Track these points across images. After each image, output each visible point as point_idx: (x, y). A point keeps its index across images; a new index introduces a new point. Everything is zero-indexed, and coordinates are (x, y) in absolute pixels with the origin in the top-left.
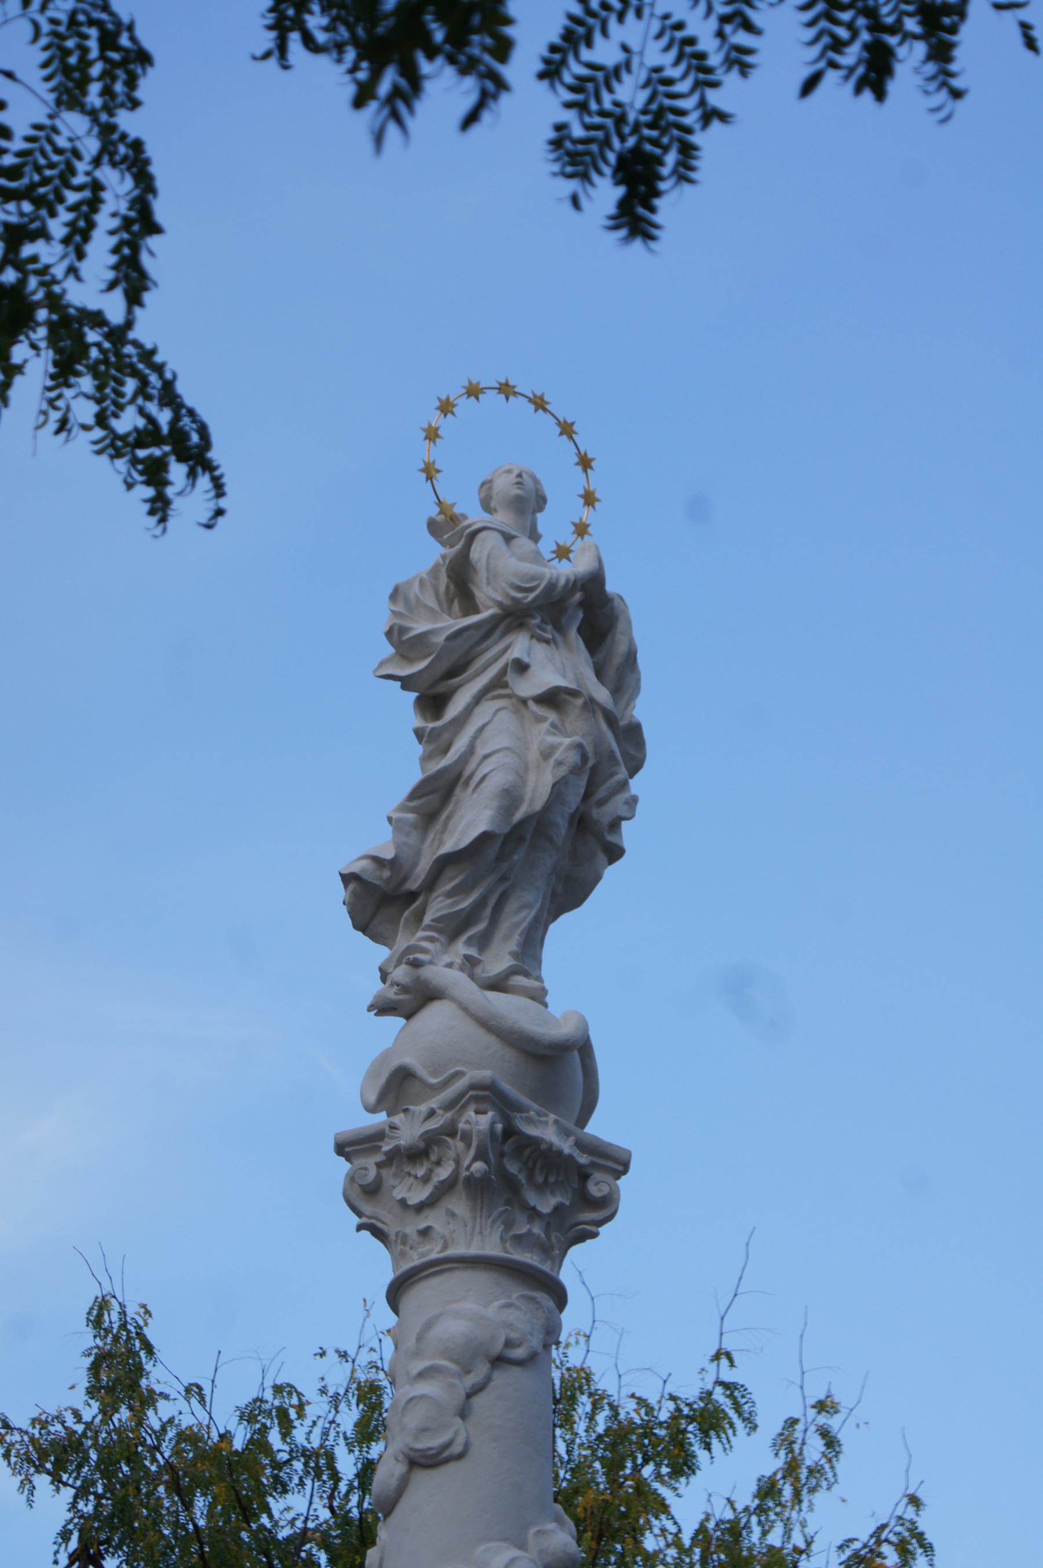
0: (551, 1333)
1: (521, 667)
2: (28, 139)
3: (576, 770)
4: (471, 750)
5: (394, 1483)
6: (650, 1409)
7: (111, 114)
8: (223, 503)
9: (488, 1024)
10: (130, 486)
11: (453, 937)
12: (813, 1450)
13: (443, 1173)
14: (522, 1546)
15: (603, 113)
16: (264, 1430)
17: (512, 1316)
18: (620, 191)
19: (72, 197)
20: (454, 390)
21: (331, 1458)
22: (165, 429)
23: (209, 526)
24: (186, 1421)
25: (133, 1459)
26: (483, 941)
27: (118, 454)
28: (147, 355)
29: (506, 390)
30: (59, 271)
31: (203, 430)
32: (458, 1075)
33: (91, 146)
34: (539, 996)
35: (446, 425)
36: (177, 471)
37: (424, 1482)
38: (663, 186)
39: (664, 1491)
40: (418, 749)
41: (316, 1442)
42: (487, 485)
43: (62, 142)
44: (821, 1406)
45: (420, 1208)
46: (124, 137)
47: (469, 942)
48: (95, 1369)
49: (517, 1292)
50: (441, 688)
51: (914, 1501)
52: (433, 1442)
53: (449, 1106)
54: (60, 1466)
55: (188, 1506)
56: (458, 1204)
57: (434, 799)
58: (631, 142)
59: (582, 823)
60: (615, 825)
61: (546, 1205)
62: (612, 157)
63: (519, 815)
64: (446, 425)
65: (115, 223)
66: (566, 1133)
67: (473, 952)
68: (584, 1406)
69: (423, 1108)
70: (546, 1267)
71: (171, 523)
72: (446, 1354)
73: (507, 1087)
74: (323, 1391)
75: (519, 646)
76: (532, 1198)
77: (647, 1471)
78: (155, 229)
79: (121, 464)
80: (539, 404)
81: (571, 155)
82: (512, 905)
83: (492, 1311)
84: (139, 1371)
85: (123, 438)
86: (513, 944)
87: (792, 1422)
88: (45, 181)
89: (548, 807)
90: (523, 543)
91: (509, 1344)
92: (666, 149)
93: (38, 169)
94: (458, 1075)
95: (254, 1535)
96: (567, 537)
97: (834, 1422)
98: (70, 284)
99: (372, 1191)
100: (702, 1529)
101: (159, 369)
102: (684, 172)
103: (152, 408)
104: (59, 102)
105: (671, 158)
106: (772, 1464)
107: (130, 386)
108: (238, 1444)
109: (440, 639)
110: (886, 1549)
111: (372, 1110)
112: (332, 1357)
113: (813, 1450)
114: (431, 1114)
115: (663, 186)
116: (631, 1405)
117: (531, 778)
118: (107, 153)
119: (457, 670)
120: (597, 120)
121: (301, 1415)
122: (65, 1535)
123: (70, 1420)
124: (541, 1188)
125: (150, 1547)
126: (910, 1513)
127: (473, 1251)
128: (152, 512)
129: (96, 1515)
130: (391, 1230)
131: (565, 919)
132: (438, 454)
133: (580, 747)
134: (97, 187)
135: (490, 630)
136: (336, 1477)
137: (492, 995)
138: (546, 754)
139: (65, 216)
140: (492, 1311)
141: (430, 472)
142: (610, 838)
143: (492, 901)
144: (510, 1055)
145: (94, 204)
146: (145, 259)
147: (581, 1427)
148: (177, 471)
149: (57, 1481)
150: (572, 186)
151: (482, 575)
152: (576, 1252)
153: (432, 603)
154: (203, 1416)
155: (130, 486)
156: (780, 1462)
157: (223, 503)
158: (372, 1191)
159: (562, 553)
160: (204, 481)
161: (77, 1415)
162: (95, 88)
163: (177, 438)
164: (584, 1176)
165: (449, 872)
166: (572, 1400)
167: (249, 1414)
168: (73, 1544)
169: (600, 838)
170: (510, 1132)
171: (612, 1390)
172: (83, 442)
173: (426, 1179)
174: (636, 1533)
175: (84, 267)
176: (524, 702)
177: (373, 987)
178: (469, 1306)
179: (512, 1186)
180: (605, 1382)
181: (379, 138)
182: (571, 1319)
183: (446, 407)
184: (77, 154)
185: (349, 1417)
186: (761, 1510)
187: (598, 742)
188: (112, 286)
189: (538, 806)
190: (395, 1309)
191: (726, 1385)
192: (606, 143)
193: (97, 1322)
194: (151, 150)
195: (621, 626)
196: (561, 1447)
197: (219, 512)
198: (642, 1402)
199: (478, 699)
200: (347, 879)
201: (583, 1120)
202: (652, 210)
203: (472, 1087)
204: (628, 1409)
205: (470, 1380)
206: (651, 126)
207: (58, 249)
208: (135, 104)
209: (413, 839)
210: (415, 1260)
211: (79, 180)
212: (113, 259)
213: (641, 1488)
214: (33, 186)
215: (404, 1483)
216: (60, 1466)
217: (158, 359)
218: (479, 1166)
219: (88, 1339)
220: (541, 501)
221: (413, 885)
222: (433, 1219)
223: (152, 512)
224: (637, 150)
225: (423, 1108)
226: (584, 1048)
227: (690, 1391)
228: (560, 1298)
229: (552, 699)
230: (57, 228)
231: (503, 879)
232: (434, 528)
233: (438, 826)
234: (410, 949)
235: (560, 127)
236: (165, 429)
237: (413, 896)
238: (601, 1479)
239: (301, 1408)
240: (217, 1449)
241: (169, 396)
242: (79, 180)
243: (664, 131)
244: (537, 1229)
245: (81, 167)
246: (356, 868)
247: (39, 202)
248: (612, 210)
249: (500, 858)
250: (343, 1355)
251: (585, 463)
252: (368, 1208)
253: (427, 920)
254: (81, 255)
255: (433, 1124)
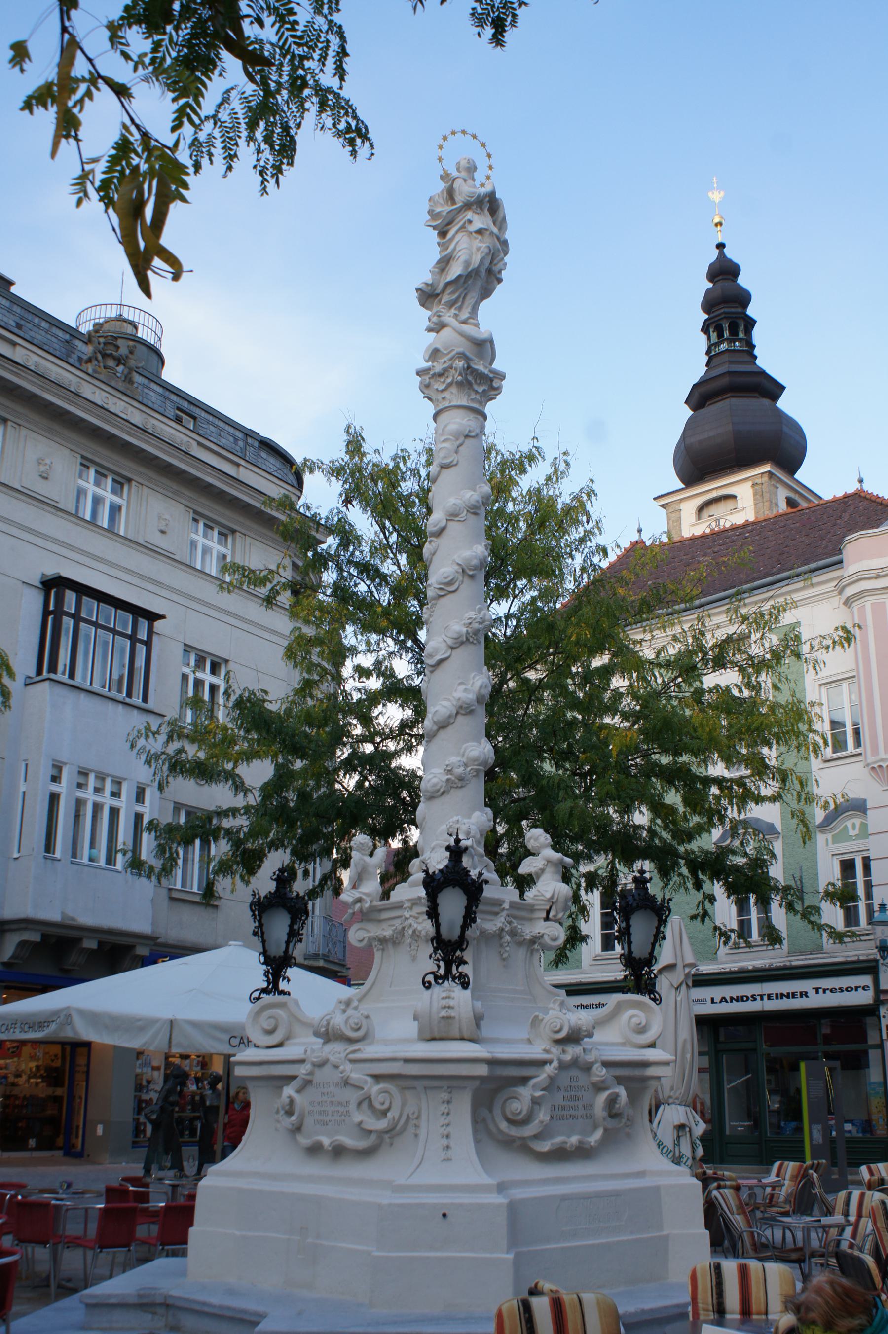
0: (483, 427)
1: (470, 222)
2: (305, 26)
3: (488, 254)
4: (455, 249)
5: (436, 473)
6: (513, 455)
7: (331, 15)
8: (373, 151)
9: (462, 334)
10: (344, 147)
11: (451, 307)
12: (562, 467)
13: (449, 380)
14: (475, 491)
15: (487, 4)
16: (398, 463)
17: (470, 423)
18: (494, 30)
19: (320, 45)
20: (458, 129)
21: (418, 471)
22: (354, 128)
23: (369, 159)
24: (375, 460)
25: (360, 472)
26: (460, 309)
27: (340, 136)
28: (347, 102)
29: (464, 132)
30: (317, 71)
31: (366, 128)
32: (453, 350)
33: (325, 27)
34: (477, 325)
35: (445, 144)
36: (358, 141)
37: (445, 472)
38: (507, 28)
39: (517, 479)
40: (439, 249)
41: (414, 466)
42: (458, 163)
43: (316, 27)
44: (564, 454)
45: (442, 391)
46: (336, 24)
47: (455, 309)
48: (347, 446)
49: (472, 416)
50: (445, 229)
51: (592, 481)
52: (447, 461)
53: (451, 359)
54: (338, 474)
55: (377, 485)
56: (454, 389)
57: (444, 264)
58: (496, 14)
59: (490, 271)
60: (500, 272)
61: (480, 389)
62: (490, 19)
63: (470, 269)
64: (445, 144)
65: (335, 53)
66: (486, 367)
67: (457, 312)
68: (494, 454)
69: (442, 361)
70: (481, 408)
71: (358, 158)
72: (451, 434)
73: (468, 354)
74: (416, 451)
75: (469, 215)
76: (476, 387)
77: (513, 473)
78: (347, 55)
79: (341, 140)
80: (474, 136)
81: (479, 19)
82: (468, 298)
83: (464, 421)
84: (360, 446)
85: (341, 131)
86: (469, 309)
87: (556, 458)
88: (311, 40)
89: (479, 266)
90: (470, 182)
91: (470, 431)
92: (508, 16)
93: (309, 36)
94: (453, 350)
95: (396, 493)
96: (484, 180)
97: (568, 458)
98: (321, 76)
99: (428, 386)
100: (529, 490)
101: (351, 107)
102: (513, 24)
103: (350, 120)
104: (315, 12)
105: (509, 19)
106: (550, 471)
107: (342, 112)
108: (391, 467)
109: (445, 213)
110: (583, 495)
111: (427, 361)
112: (418, 440)
113: (562, 467)
114: (445, 362)
115: (507, 28)
116: (508, 454)
117: (474, 257)
118: (330, 29)
119: (450, 223)
120: (485, 7)
121: (409, 458)
122: (341, 495)
123: (341, 461)
124: (479, 384)
125: (366, 498)
126: (590, 484)
127: (459, 403)
128: (351, 155)
129: (350, 489)
130: (433, 398)
131: (485, 301)
132: (442, 153)
133: (489, 247)
134: (328, 41)
135: (460, 210)
136: (420, 476)
137: (463, 325)
138: (478, 249)
139: (318, 52)
140: (464, 421)
141: (440, 159)
142: (498, 276)
143: (462, 296)
144: (468, 344)
145: (327, 47)
146: (345, 65)
147: (493, 461)
148: (358, 141)
149: (338, 479)
150: (478, 29)
151: (457, 193)
152: (489, 403)
153: (441, 201)
154: (380, 459)
155: (344, 147)
156: (552, 470)
157: (373, 151)
158: (428, 386)
159: (482, 185)
160: (367, 144)
161: (343, 460)
162: (326, 7)
163: (358, 130)
164: (492, 380)
165: (449, 287)
166: (490, 453)
167: (394, 458)
168: (343, 497)
169: (495, 275)
170: (469, 367)
171: (502, 450)
172: (329, 134)
173: (444, 382)
174: (509, 491)
175: (325, 69)
176: (471, 233)
177: (427, 323)
178: (458, 420)
179: (470, 384)
180: (499, 447)
181: (415, 9)
182: (488, 423)
183: (445, 138)
184: (321, 30)
185: (423, 459)
186: (546, 484)
187: (494, 246)
188: (335, 75)
189: (476, 266)
190: (435, 421)
191: (536, 447)
192: (489, 14)
193: (348, 432)
194: (344, 28)
195: (501, 208)
196: (487, 467)
197: (373, 154)
198: (511, 452)
199: (457, 232)
200: (418, 290)
201: (491, 364)
202: (503, 37)
203: (458, 353)
204: (507, 455)
205: (458, 443)
206: (503, 8)
207: (317, 63)
208: (339, 10)
209: (437, 277)
210: (441, 407)
211: (322, 39)
212: (335, 66)
213: (511, 477)
214: (307, 42)
215: (439, 473)
216: (338, 474)
217: (350, 103)
218: (460, 378)
219: (345, 437)
220: (475, 168)
221: (438, 291)
222: (446, 394)
223: (351, 155)
224: (498, 17)
225: (442, 361)
226: (491, 342)
227: (525, 450)
228: (485, 417)
229: (480, 232)
230: (316, 56)
231: (466, 289)
232: (442, 177)
233: (445, 273)
234: (437, 312)
235: (473, 9)
236: (354, 128)
237: (438, 295)
238: (499, 476)
239: (409, 456)
240: (384, 468)
241: (355, 117)
242: (322, 39)
243: (507, 10)
244: (478, 397)
245: (323, 35)
246: (420, 287)
247: (309, 48)
248: (491, 37)
249: (465, 282)
250: (421, 440)
251: (489, 156)
252: (426, 391)
253: (443, 302)
254: (324, 65)
255: (446, 365)
